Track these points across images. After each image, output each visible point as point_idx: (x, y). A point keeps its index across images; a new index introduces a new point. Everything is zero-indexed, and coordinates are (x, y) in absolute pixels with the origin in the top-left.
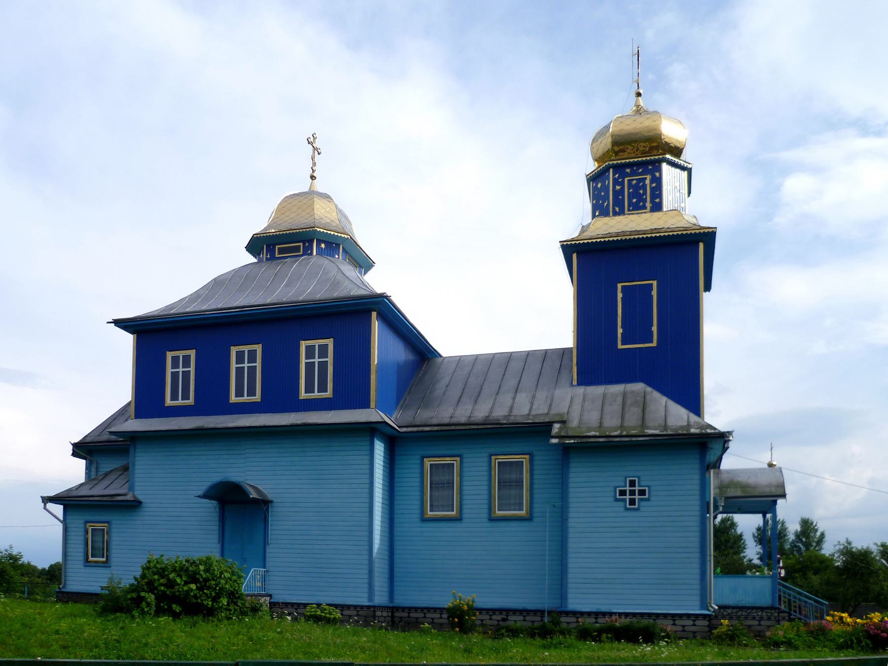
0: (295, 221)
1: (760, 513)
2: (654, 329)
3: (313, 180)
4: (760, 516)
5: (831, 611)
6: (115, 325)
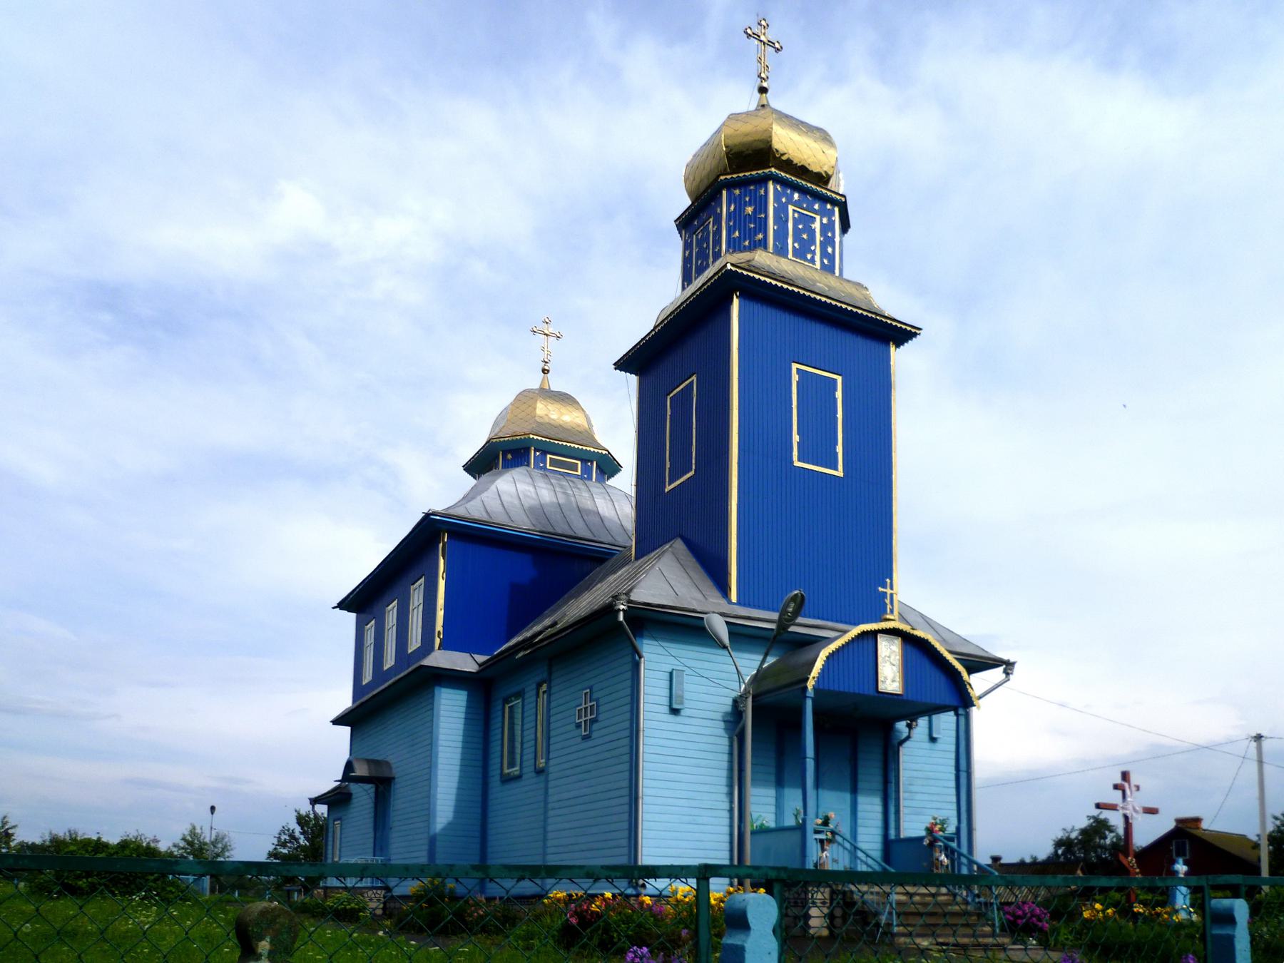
0: (519, 429)
1: (950, 711)
2: (839, 449)
3: (545, 373)
4: (952, 713)
5: (1185, 863)
6: (340, 609)
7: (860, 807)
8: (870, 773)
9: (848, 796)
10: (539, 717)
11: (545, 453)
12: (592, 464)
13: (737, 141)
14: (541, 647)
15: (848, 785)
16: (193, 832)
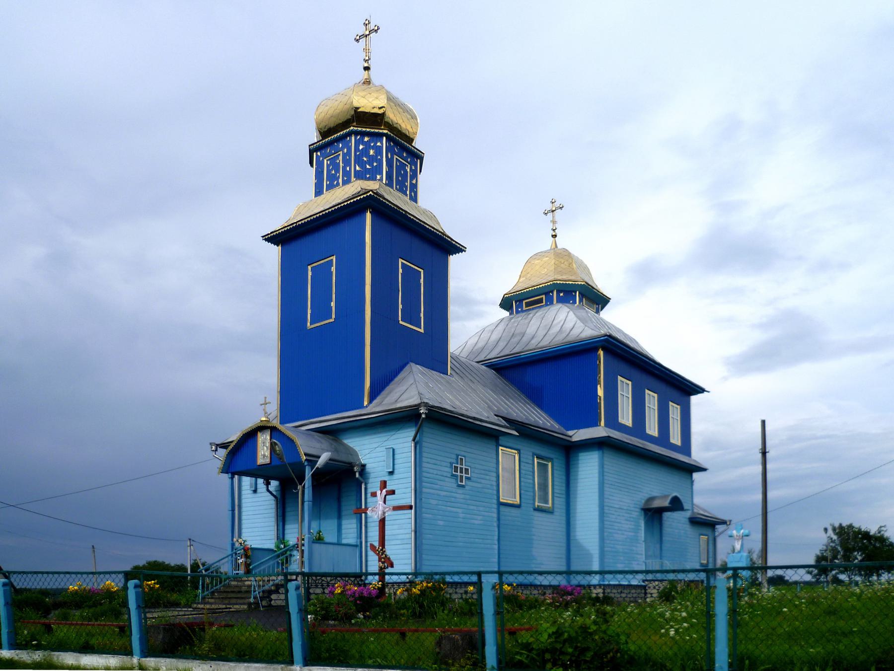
3: (553, 238)
7: (344, 527)
8: (348, 506)
9: (335, 521)
10: (428, 484)
11: (521, 301)
12: (553, 293)
13: (323, 124)
14: (528, 427)
15: (336, 514)
16: (816, 554)
